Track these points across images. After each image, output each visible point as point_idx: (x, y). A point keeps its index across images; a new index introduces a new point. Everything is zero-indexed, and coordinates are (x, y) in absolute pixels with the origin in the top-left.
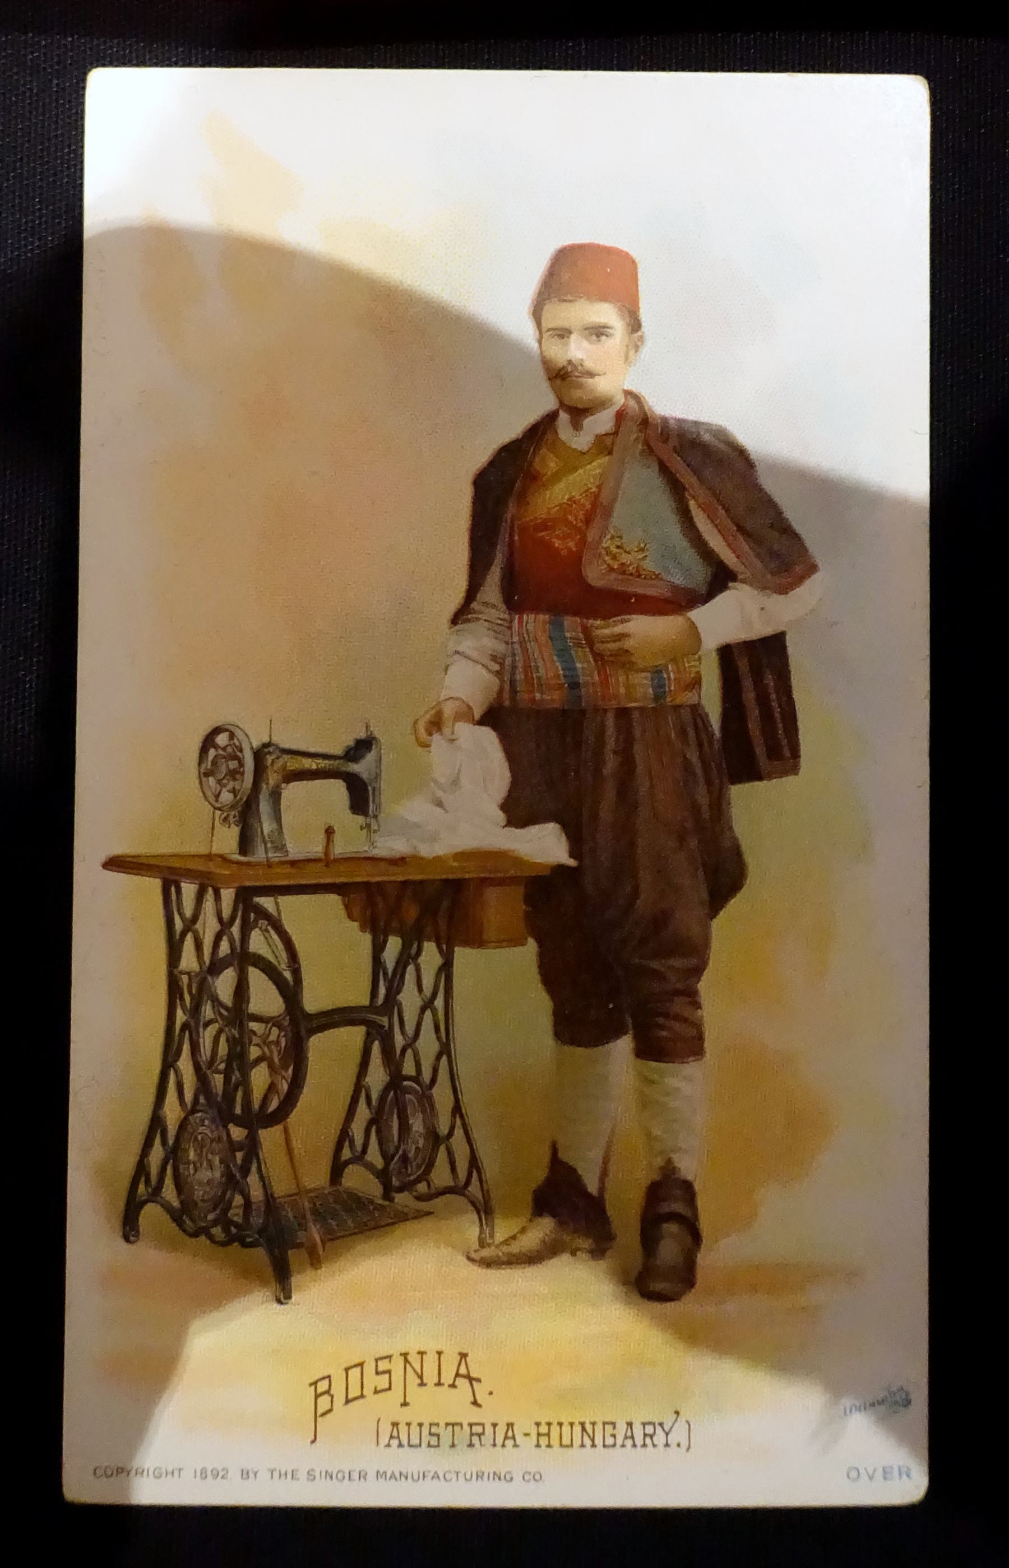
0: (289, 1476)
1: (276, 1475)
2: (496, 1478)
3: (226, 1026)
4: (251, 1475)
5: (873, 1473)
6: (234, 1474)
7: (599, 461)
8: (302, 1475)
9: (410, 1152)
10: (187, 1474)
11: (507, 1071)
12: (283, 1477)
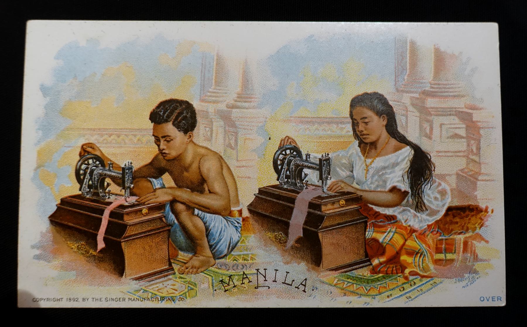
0: (99, 300)
1: (94, 300)
3: (373, 267)
4: (86, 300)
5: (489, 299)
6: (80, 300)
7: (237, 214)
8: (103, 299)
9: (234, 252)
10: (90, 300)
11: (436, 199)
12: (97, 300)
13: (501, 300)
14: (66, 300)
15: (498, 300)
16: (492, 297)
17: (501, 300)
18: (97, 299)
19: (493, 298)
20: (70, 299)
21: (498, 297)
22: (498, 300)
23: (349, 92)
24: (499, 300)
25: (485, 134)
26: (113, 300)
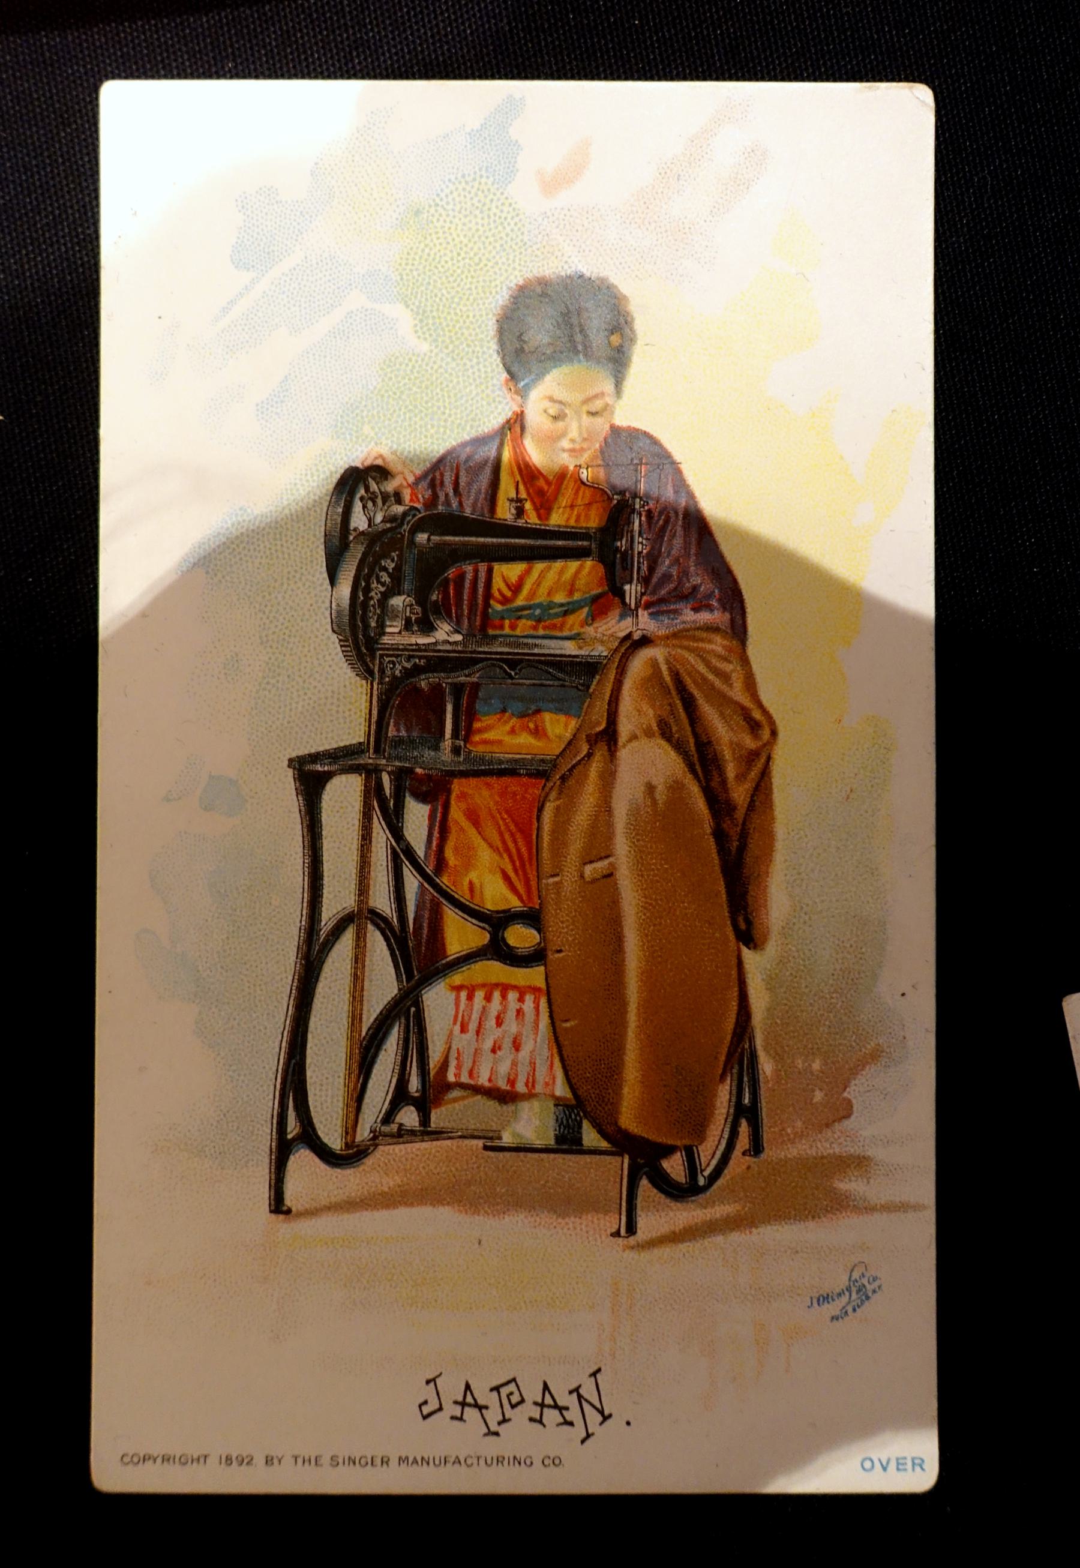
1: (300, 1461)
2: (351, 1463)
4: (275, 1461)
12: (307, 1464)
13: (923, 1469)
14: (217, 1461)
15: (913, 1469)
16: (897, 1459)
17: (923, 1469)
18: (307, 1458)
19: (901, 1461)
20: (229, 1460)
21: (913, 1459)
22: (913, 1469)
23: (450, 263)
24: (918, 1469)
25: (266, 1028)
26: (354, 1463)
